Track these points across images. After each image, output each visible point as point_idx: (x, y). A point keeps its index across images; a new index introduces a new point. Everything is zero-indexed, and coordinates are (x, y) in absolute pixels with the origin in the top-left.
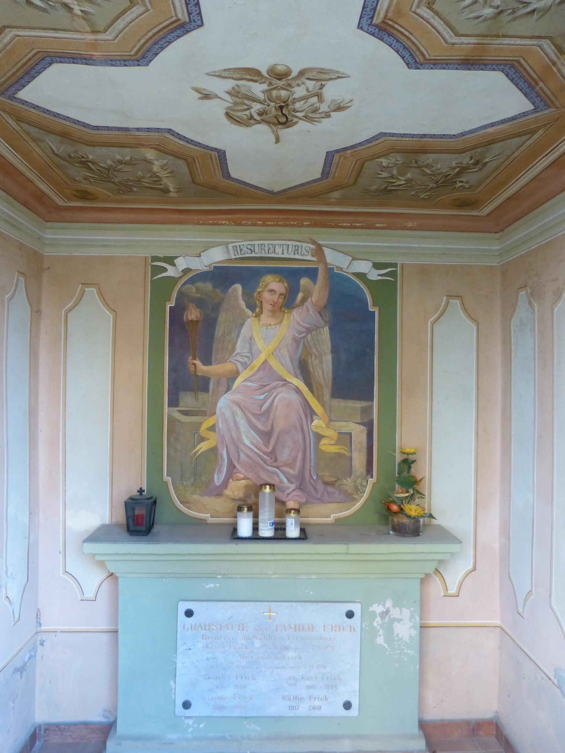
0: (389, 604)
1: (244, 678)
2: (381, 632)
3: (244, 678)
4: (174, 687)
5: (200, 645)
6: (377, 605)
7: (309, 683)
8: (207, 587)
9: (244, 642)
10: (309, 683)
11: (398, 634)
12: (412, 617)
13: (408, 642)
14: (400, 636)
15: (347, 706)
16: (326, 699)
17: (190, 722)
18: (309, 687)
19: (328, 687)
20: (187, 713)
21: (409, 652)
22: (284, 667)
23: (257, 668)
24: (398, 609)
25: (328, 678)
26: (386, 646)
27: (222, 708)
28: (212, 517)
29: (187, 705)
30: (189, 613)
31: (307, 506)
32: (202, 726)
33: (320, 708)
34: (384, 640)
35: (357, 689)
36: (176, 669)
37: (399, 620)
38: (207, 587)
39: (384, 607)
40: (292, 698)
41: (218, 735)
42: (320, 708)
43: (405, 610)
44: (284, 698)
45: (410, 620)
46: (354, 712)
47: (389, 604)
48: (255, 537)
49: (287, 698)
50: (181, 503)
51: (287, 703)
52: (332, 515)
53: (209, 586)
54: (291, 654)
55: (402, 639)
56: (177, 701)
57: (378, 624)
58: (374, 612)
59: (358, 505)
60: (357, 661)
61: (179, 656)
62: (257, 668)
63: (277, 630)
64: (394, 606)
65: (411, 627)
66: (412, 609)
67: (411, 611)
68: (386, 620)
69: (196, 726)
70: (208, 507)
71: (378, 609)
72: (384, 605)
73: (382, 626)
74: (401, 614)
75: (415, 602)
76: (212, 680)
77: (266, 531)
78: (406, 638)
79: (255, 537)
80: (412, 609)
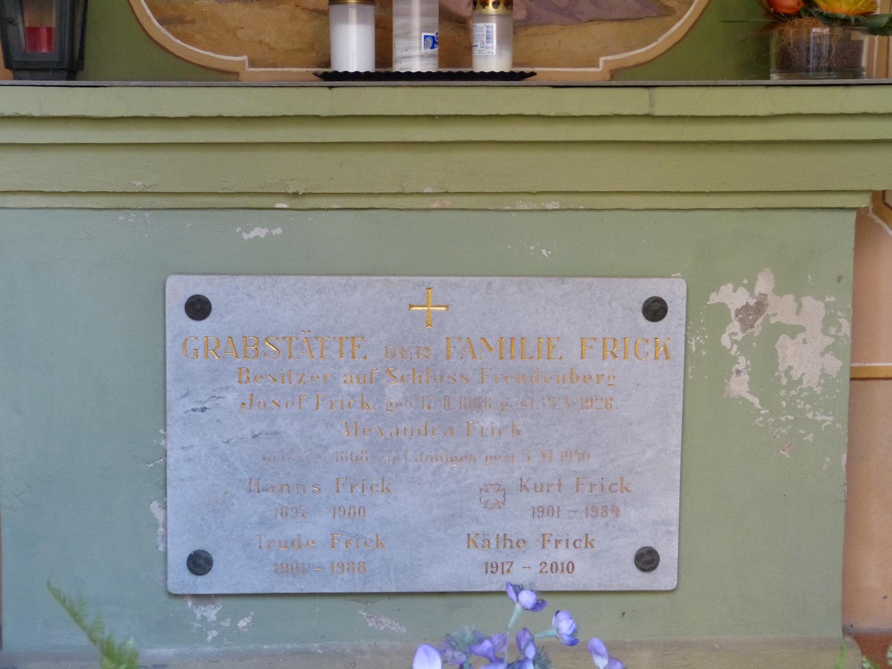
0: (764, 284)
1: (358, 489)
2: (742, 363)
3: (358, 489)
4: (161, 521)
5: (231, 398)
6: (730, 286)
7: (540, 499)
8: (246, 236)
9: (355, 388)
10: (540, 499)
11: (791, 368)
12: (829, 322)
13: (818, 390)
14: (796, 375)
15: (647, 560)
16: (589, 544)
17: (211, 612)
18: (540, 511)
19: (592, 511)
20: (202, 584)
21: (819, 418)
22: (467, 457)
23: (396, 459)
24: (789, 298)
25: (592, 486)
26: (756, 401)
27: (298, 569)
28: (252, 64)
29: (199, 563)
30: (198, 308)
31: (530, 30)
32: (242, 623)
33: (570, 567)
34: (749, 383)
35: (675, 515)
36: (165, 468)
37: (793, 331)
38: (246, 236)
39: (752, 295)
40: (493, 541)
41: (289, 646)
42: (570, 567)
43: (808, 302)
44: (470, 541)
45: (825, 332)
46: (664, 577)
47: (764, 284)
48: (384, 73)
49: (479, 541)
50: (161, 22)
51: (481, 556)
52: (602, 59)
53: (252, 234)
54: (488, 420)
55: (800, 381)
56: (171, 554)
57: (734, 342)
58: (722, 307)
59: (678, 28)
60: (676, 440)
61: (175, 431)
62: (396, 459)
63: (448, 358)
64: (779, 291)
65: (827, 349)
66: (832, 299)
67: (827, 306)
68: (757, 329)
69: (227, 624)
70: (240, 33)
71: (733, 297)
72: (750, 288)
73: (744, 346)
74: (798, 313)
75: (840, 278)
76: (269, 494)
77: (414, 56)
78: (812, 380)
79: (384, 73)
80: (832, 299)
